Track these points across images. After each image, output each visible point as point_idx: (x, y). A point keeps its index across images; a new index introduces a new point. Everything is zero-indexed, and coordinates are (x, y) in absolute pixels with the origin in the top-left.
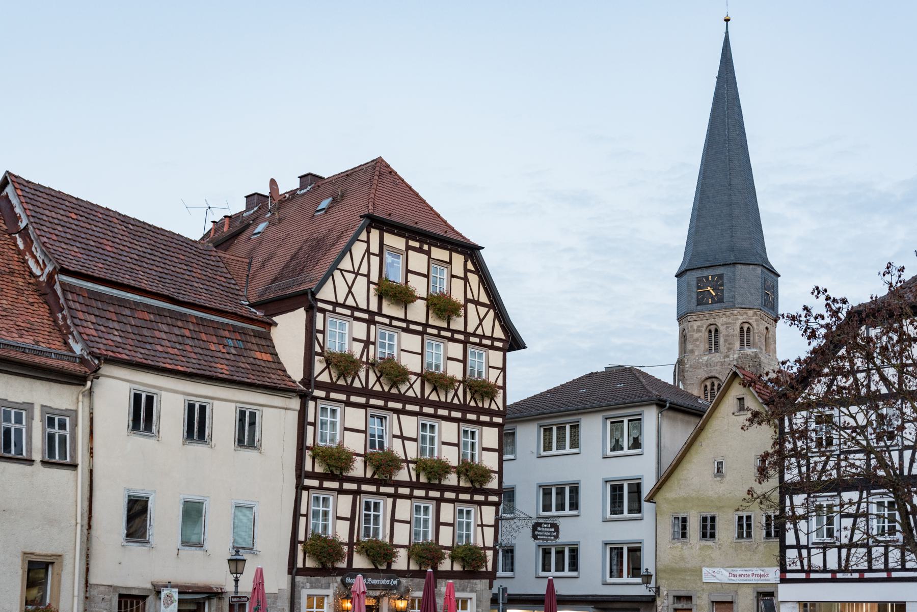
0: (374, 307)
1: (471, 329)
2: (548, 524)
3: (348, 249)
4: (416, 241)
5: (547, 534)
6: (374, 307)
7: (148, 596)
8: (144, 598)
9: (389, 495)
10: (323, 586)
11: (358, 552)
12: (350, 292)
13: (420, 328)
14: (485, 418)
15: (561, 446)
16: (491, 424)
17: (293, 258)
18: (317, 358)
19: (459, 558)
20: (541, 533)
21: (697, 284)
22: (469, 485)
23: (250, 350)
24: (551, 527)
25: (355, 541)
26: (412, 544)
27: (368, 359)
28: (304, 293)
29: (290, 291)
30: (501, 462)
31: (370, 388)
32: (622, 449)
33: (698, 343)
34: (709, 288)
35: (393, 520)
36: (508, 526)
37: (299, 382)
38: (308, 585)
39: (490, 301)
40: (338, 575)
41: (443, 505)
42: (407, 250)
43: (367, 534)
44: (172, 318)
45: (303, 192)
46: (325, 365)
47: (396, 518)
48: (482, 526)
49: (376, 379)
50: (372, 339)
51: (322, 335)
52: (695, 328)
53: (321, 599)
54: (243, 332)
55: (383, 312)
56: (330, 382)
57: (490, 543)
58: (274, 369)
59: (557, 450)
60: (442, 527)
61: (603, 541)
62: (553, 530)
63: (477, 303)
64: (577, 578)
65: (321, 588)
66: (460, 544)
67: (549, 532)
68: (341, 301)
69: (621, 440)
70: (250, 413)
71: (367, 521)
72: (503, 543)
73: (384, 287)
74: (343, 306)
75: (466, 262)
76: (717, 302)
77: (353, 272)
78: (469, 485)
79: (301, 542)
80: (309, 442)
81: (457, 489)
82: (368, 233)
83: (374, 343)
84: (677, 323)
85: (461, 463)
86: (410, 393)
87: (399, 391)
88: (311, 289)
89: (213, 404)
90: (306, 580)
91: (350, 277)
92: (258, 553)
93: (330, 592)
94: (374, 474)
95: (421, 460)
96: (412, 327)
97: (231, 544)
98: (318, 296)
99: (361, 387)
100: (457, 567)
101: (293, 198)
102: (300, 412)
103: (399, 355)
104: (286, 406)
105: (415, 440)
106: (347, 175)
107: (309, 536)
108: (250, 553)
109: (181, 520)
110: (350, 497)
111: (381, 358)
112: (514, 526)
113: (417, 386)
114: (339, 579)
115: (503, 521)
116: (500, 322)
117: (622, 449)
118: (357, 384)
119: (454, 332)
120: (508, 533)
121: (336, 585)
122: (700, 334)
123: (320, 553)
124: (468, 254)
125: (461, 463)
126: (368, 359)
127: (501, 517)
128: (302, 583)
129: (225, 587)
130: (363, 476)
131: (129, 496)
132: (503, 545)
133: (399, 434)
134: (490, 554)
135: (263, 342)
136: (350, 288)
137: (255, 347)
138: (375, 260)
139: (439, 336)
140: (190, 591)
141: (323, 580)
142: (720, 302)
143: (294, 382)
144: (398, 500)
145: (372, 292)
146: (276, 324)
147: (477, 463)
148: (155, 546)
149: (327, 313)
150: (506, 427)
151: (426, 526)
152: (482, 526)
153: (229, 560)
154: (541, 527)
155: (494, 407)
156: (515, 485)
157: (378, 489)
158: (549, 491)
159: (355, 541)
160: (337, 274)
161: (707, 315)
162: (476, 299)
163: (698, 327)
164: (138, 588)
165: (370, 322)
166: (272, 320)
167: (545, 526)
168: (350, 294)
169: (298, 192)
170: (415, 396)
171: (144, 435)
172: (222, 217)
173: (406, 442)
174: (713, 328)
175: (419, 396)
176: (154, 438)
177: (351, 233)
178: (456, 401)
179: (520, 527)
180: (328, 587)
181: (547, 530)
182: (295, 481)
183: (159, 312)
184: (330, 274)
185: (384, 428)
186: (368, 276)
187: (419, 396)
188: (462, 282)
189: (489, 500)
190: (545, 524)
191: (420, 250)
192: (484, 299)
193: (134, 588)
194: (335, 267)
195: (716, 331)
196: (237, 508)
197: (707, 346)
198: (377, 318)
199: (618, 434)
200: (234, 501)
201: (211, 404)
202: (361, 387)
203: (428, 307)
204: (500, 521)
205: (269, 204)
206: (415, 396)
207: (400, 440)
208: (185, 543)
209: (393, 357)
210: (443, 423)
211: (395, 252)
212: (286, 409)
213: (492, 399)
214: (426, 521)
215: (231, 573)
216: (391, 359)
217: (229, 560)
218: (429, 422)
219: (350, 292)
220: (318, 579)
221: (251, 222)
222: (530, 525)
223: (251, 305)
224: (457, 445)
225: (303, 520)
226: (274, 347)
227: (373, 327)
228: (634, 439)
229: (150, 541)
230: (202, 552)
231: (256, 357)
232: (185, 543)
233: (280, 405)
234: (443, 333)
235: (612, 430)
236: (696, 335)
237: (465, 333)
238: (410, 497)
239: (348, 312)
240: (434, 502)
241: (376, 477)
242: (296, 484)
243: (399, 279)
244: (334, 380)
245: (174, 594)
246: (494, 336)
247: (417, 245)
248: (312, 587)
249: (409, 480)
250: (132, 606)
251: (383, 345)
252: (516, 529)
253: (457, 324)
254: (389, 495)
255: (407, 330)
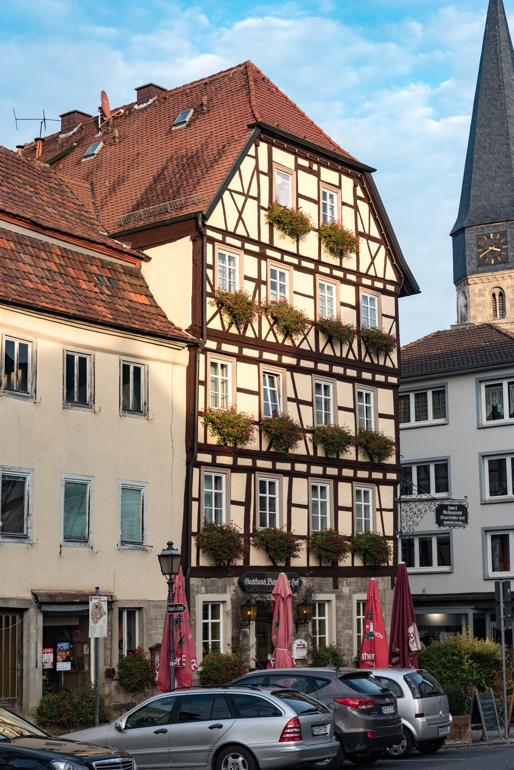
0: (265, 239)
1: (363, 269)
2: (455, 506)
3: (236, 168)
4: (306, 158)
5: (454, 518)
6: (265, 239)
7: (27, 609)
8: (21, 611)
9: (285, 473)
10: (220, 589)
11: (255, 545)
12: (240, 218)
13: (311, 266)
14: (379, 378)
15: (421, 415)
16: (386, 385)
17: (157, 179)
18: (208, 299)
19: (360, 550)
20: (447, 518)
21: (477, 242)
22: (367, 460)
23: (124, 290)
24: (458, 510)
25: (251, 532)
26: (311, 534)
27: (260, 302)
28: (194, 217)
29: (168, 217)
30: (397, 430)
31: (263, 338)
32: (502, 417)
33: (480, 308)
34: (490, 248)
35: (290, 505)
36: (408, 510)
37: (186, 330)
38: (203, 589)
39: (381, 234)
40: (235, 576)
41: (341, 485)
42: (296, 170)
43: (263, 524)
44: (34, 248)
45: (141, 106)
46: (215, 309)
47: (293, 502)
48: (381, 510)
49: (269, 327)
50: (264, 278)
51: (211, 271)
52: (477, 291)
53: (215, 607)
54: (113, 269)
55: (276, 245)
56: (222, 330)
57: (389, 532)
58: (153, 314)
59: (416, 421)
60: (340, 513)
61: (482, 528)
62: (460, 513)
63: (369, 238)
64: (451, 573)
65: (217, 592)
66: (360, 533)
67: (456, 516)
68: (231, 229)
69: (499, 406)
70: (135, 368)
71: (263, 506)
72: (403, 531)
73: (276, 213)
74: (233, 235)
75: (355, 186)
76: (501, 263)
77: (242, 194)
78: (367, 460)
79: (194, 534)
80: (201, 407)
81: (355, 465)
82: (257, 146)
83: (265, 283)
84: (454, 287)
85: (358, 433)
86: (305, 346)
87: (293, 342)
88: (201, 212)
89: (94, 356)
90: (200, 583)
91: (240, 199)
92: (149, 548)
93: (227, 597)
94: (269, 448)
95: (318, 428)
96: (304, 264)
97: (119, 538)
98: (209, 223)
99: (254, 337)
100: (358, 563)
101: (130, 114)
102: (188, 368)
103: (291, 298)
104: (173, 361)
105: (310, 404)
106: (206, 83)
107: (202, 526)
108: (140, 549)
109: (63, 506)
110: (244, 476)
111: (273, 302)
112: (415, 510)
113: (311, 337)
114: (236, 580)
115: (403, 505)
116: (392, 261)
117: (502, 417)
118: (250, 334)
119: (347, 271)
120: (408, 518)
121: (233, 588)
122: (483, 298)
123: (219, 547)
124: (358, 178)
125: (358, 433)
126: (260, 302)
127: (400, 498)
128: (197, 586)
129: (115, 594)
130: (259, 449)
131: (3, 476)
132: (404, 534)
133: (293, 396)
134: (391, 543)
135: (135, 281)
136: (240, 213)
137: (127, 287)
138: (264, 180)
139: (331, 276)
140: (78, 600)
141: (220, 582)
142: (504, 263)
143: (180, 330)
144: (295, 480)
145: (264, 220)
146: (148, 259)
147: (373, 430)
148: (35, 541)
149: (216, 243)
150: (402, 388)
151: (324, 512)
152: (381, 510)
153: (159, 556)
154: (447, 510)
155: (389, 364)
156: (449, 456)
157: (274, 465)
158: (408, 471)
159: (251, 532)
160: (226, 195)
161: (490, 277)
162: (367, 232)
163: (480, 290)
164: (16, 599)
165: (261, 256)
166: (143, 254)
167: (452, 508)
168: (241, 221)
169: (136, 107)
170: (309, 349)
171: (19, 396)
172: (33, 140)
173: (301, 406)
174: (497, 292)
175: (314, 350)
176: (30, 400)
177: (239, 148)
178: (351, 357)
179: (423, 511)
180: (224, 591)
181: (454, 513)
182: (185, 456)
183: (19, 240)
184: (219, 197)
185: (276, 389)
186: (258, 199)
187: (314, 350)
188: (352, 211)
189: (388, 478)
190: (452, 506)
191: (309, 170)
192: (375, 233)
193: (11, 599)
194: (225, 187)
195: (501, 294)
196: (128, 493)
197: (491, 311)
198: (269, 252)
199: (495, 401)
200: (121, 482)
201: (92, 356)
202: (254, 337)
203: (320, 240)
204: (399, 505)
205: (100, 122)
206: (309, 349)
207: (295, 404)
208: (68, 538)
209: (285, 301)
210: (338, 383)
211: (285, 171)
212: (174, 364)
213: (387, 355)
214: (324, 504)
215: (164, 574)
216: (283, 304)
217: (159, 556)
218: (323, 381)
219: (240, 218)
220: (213, 581)
221: (75, 144)
222: (434, 508)
223: (114, 236)
224: (353, 410)
225: (195, 505)
226: (147, 287)
227: (263, 263)
228: (493, 407)
229: (29, 535)
230: (88, 549)
231: (132, 299)
232: (68, 538)
233: (167, 359)
234: (336, 273)
235: (487, 396)
236: (478, 300)
237: (357, 273)
238: (306, 475)
239: (238, 243)
240: (332, 482)
241: (272, 450)
242: (187, 460)
243: (290, 205)
244: (226, 328)
245: (102, 603)
246: (386, 278)
247: (305, 163)
248: (207, 592)
249: (306, 454)
250: (14, 621)
251: (274, 286)
252: (418, 513)
253: (349, 263)
254: (285, 473)
255: (298, 268)
